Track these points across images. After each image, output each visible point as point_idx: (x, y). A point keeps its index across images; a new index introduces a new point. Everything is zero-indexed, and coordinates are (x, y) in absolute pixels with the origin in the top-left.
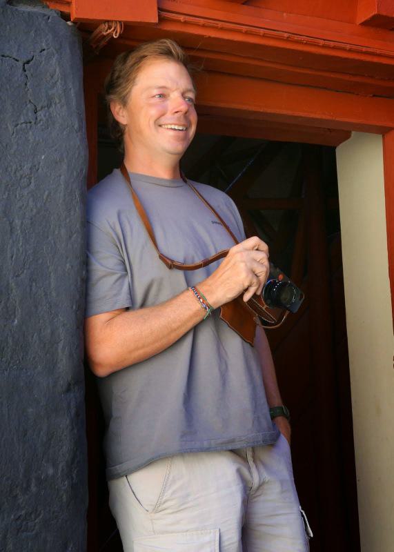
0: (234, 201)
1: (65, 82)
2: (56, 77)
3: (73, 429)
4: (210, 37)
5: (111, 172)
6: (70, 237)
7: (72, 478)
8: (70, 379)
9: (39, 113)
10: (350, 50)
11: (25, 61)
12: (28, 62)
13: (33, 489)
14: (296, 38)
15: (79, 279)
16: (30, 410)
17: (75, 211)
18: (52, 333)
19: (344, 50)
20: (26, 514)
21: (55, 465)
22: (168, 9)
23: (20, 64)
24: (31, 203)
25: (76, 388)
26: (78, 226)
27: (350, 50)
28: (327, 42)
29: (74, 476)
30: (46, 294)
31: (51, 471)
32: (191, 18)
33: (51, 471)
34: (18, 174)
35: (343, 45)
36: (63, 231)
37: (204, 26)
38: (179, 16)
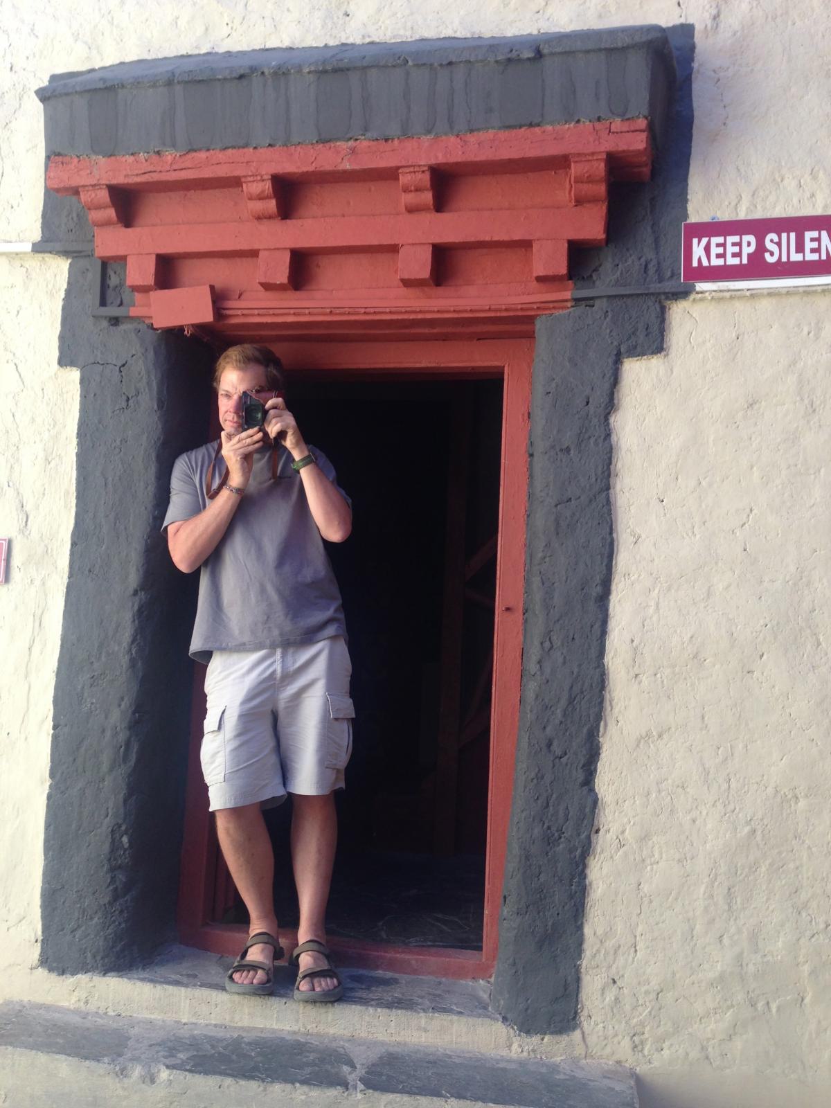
0: (220, 423)
1: (149, 376)
2: (142, 374)
3: (134, 621)
4: (267, 323)
5: (202, 446)
6: (146, 488)
7: (132, 654)
8: (135, 586)
9: (130, 402)
10: (390, 312)
11: (120, 365)
12: (123, 365)
13: (103, 659)
14: (338, 311)
15: (151, 517)
16: (107, 607)
17: (151, 468)
18: (127, 555)
19: (434, 312)
20: (98, 675)
21: (120, 644)
22: (233, 307)
23: (117, 368)
24: (120, 466)
25: (143, 593)
26: (153, 479)
27: (390, 312)
28: (311, 310)
29: (133, 652)
30: (125, 528)
31: (116, 648)
32: (300, 310)
33: (116, 648)
34: (113, 446)
35: (400, 309)
36: (142, 483)
37: (349, 313)
38: (360, 309)
